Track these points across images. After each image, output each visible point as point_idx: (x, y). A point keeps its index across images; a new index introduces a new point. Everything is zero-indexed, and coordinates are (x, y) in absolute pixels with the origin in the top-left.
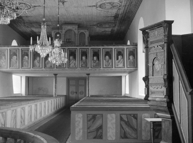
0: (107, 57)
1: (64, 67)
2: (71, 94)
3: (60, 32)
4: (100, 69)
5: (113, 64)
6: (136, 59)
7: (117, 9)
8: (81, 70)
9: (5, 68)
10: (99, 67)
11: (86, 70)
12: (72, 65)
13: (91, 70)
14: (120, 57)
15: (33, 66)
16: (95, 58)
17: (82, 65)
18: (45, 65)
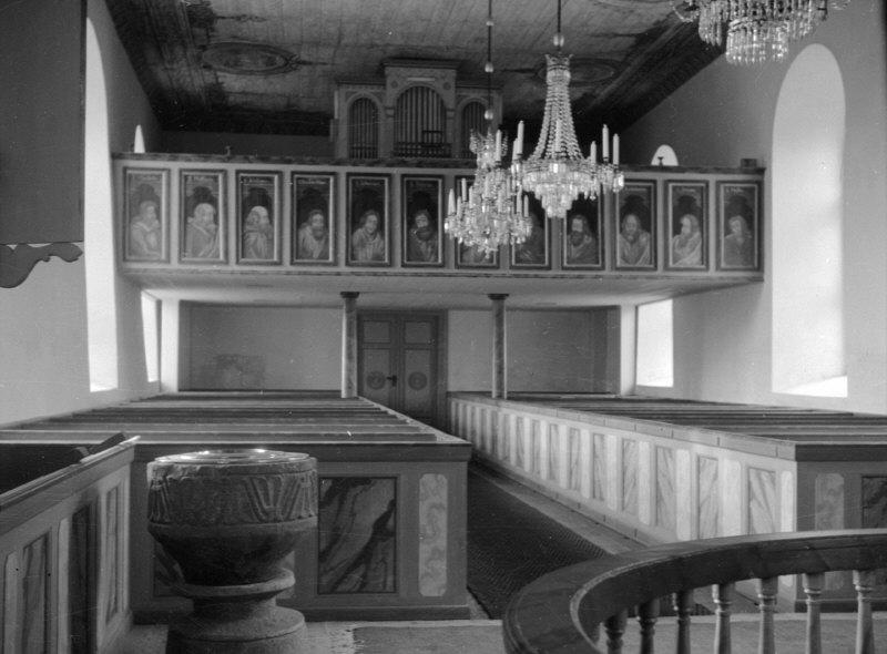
0: (632, 220)
1: (440, 261)
3: (375, 99)
4: (599, 273)
5: (656, 251)
8: (517, 276)
9: (159, 261)
10: (598, 263)
11: (536, 276)
12: (365, 254)
13: (562, 277)
14: (686, 221)
15: (292, 256)
17: (521, 256)
18: (353, 250)
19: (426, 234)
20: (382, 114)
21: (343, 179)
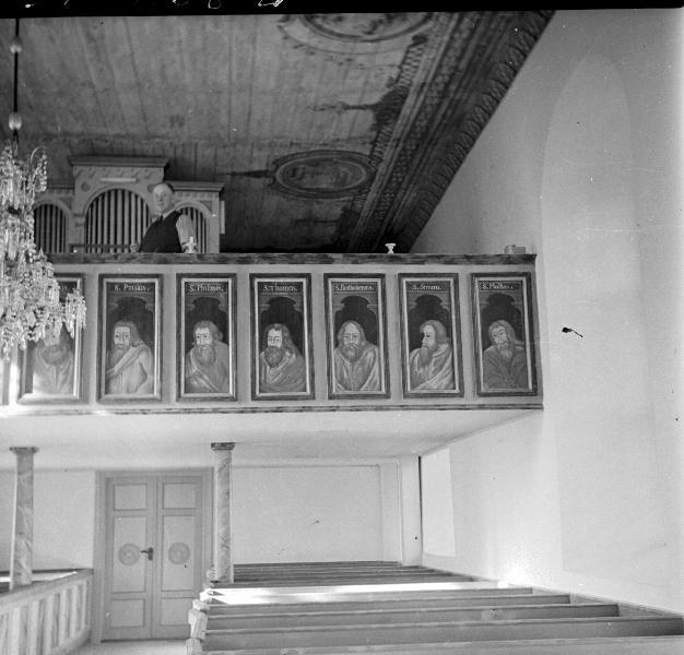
2: (170, 558)
3: (62, 206)
6: (528, 343)
7: (408, 39)
10: (305, 390)
16: (276, 336)
19: (58, 355)
20: (71, 224)
21: (317, 287)
